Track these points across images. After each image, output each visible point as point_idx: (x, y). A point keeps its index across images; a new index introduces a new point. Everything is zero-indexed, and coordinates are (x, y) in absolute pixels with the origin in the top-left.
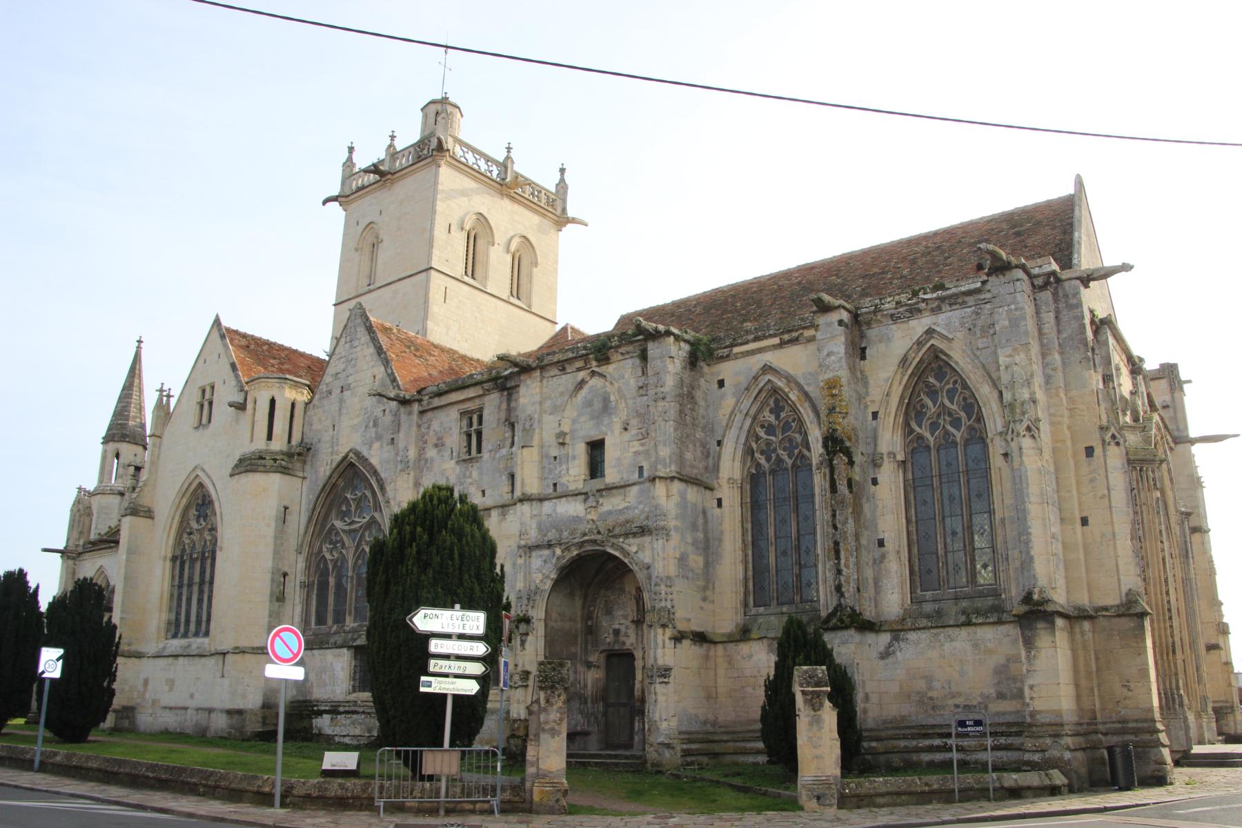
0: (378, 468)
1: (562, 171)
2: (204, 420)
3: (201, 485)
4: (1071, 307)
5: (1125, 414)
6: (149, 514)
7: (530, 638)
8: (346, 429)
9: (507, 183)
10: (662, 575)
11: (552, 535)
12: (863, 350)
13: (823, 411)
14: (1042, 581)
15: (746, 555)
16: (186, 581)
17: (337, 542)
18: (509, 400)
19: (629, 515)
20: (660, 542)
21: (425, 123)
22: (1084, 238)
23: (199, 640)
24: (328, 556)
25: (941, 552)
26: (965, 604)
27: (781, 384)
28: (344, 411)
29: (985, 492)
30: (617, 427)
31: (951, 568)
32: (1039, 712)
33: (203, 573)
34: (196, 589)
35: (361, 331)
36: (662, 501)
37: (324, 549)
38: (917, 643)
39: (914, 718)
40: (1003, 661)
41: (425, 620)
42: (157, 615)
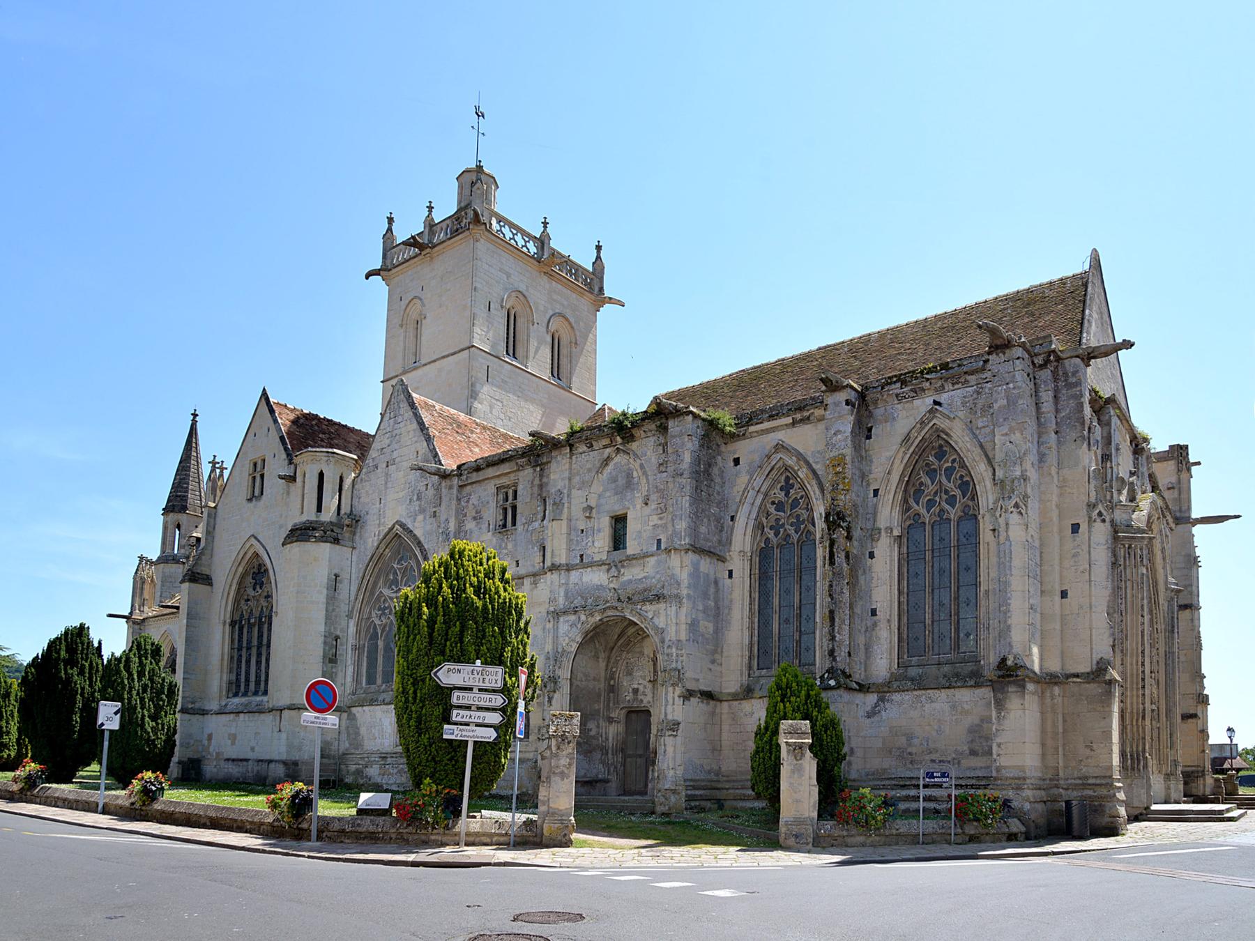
0: (422, 539)
1: (599, 248)
2: (257, 493)
3: (257, 555)
4: (1069, 386)
5: (1120, 492)
6: (207, 580)
7: (557, 696)
8: (390, 501)
9: (547, 259)
10: (674, 639)
11: (578, 602)
12: (870, 430)
13: (827, 485)
14: (1017, 649)
15: (752, 623)
16: (245, 644)
17: (385, 608)
18: (541, 476)
19: (647, 584)
20: (674, 608)
21: (460, 194)
22: (1095, 315)
23: (258, 698)
24: (377, 622)
25: (928, 621)
26: (946, 669)
27: (791, 461)
28: (389, 485)
29: (973, 568)
30: (639, 503)
31: (936, 637)
32: (1005, 767)
33: (260, 636)
34: (254, 651)
35: (404, 406)
36: (677, 571)
37: (374, 614)
38: (901, 703)
40: (977, 721)
41: (448, 674)
42: (217, 676)
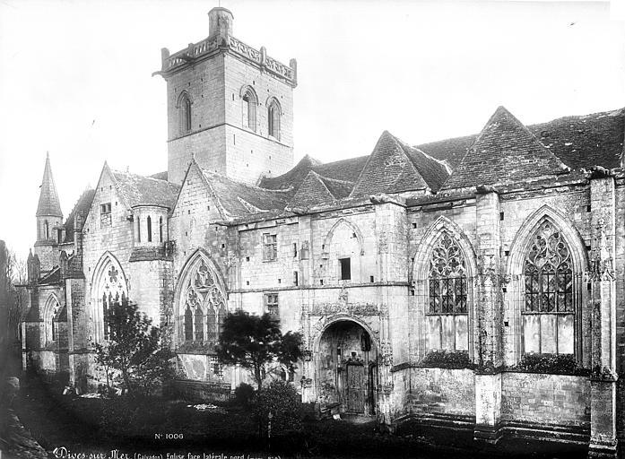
39: (114, 276)
